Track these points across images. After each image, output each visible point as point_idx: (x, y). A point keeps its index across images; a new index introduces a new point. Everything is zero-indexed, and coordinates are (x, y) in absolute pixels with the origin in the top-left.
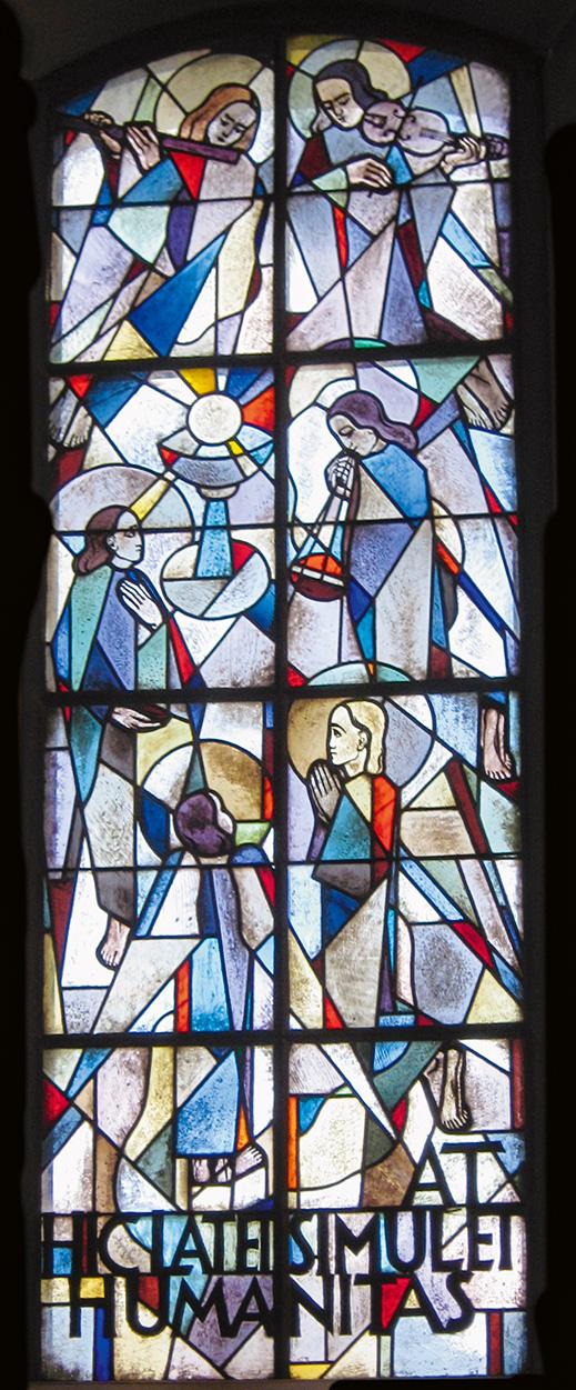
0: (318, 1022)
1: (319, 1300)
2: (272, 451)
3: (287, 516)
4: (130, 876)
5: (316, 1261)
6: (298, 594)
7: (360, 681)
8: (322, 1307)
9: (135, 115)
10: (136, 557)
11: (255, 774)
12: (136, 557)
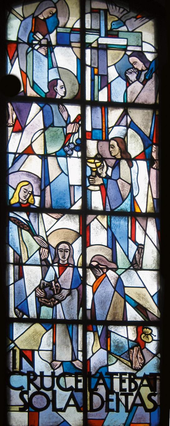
0: (112, 406)
1: (24, 360)
2: (63, 105)
3: (159, 95)
4: (106, 368)
5: (51, 403)
6: (141, 50)
7: (82, 394)
8: (31, 384)
9: (72, 131)
10: (63, 95)
11: (116, 328)
12: (63, 95)
